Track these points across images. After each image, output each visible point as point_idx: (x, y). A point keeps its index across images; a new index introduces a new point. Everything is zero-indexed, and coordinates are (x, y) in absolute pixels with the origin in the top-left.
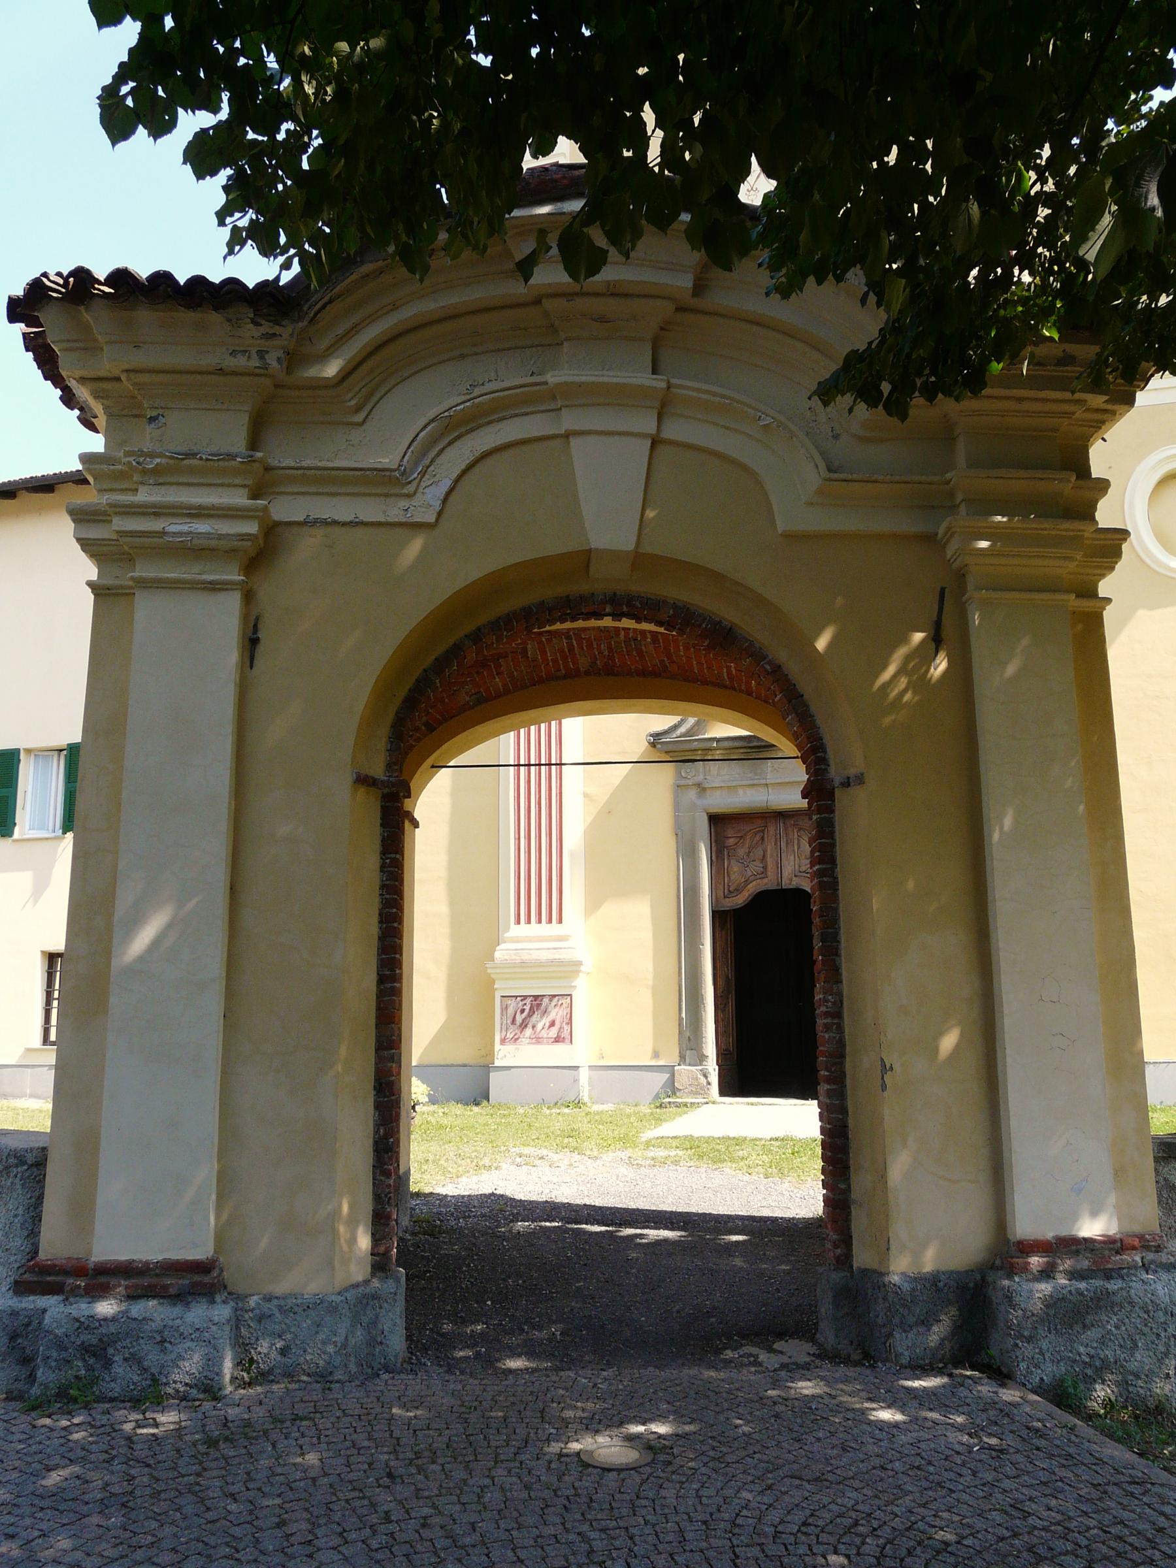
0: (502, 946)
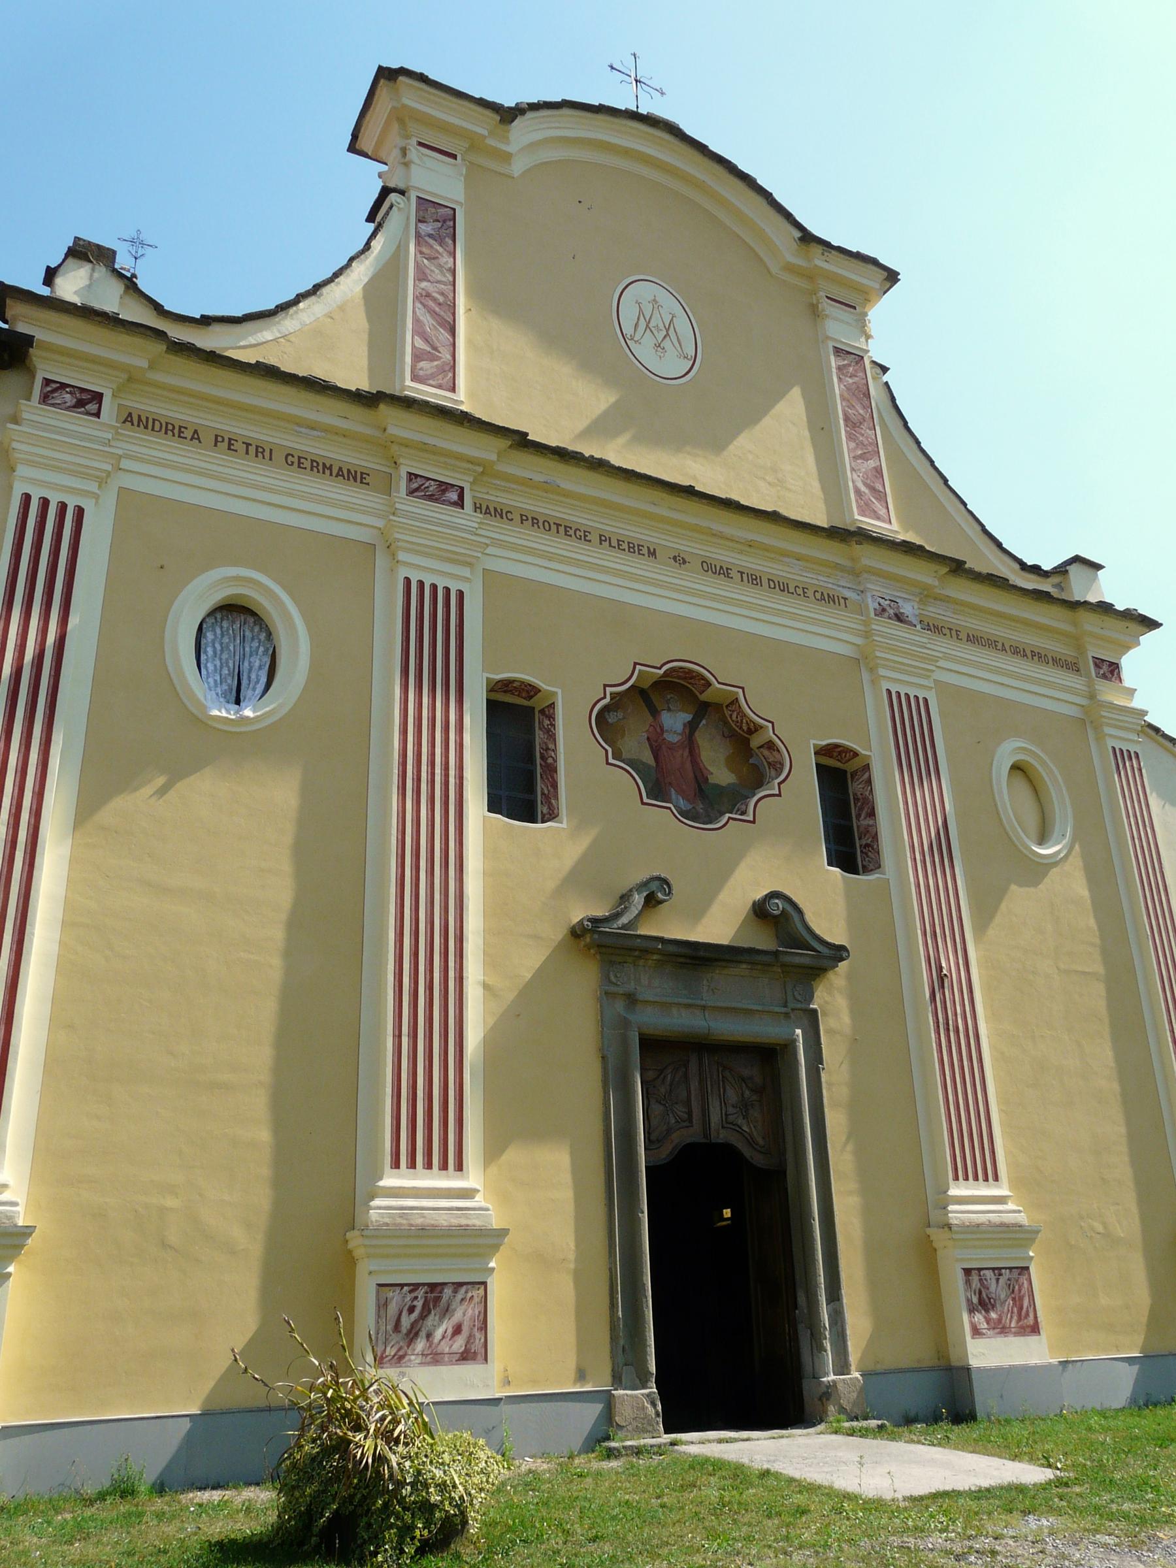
0: (377, 1202)
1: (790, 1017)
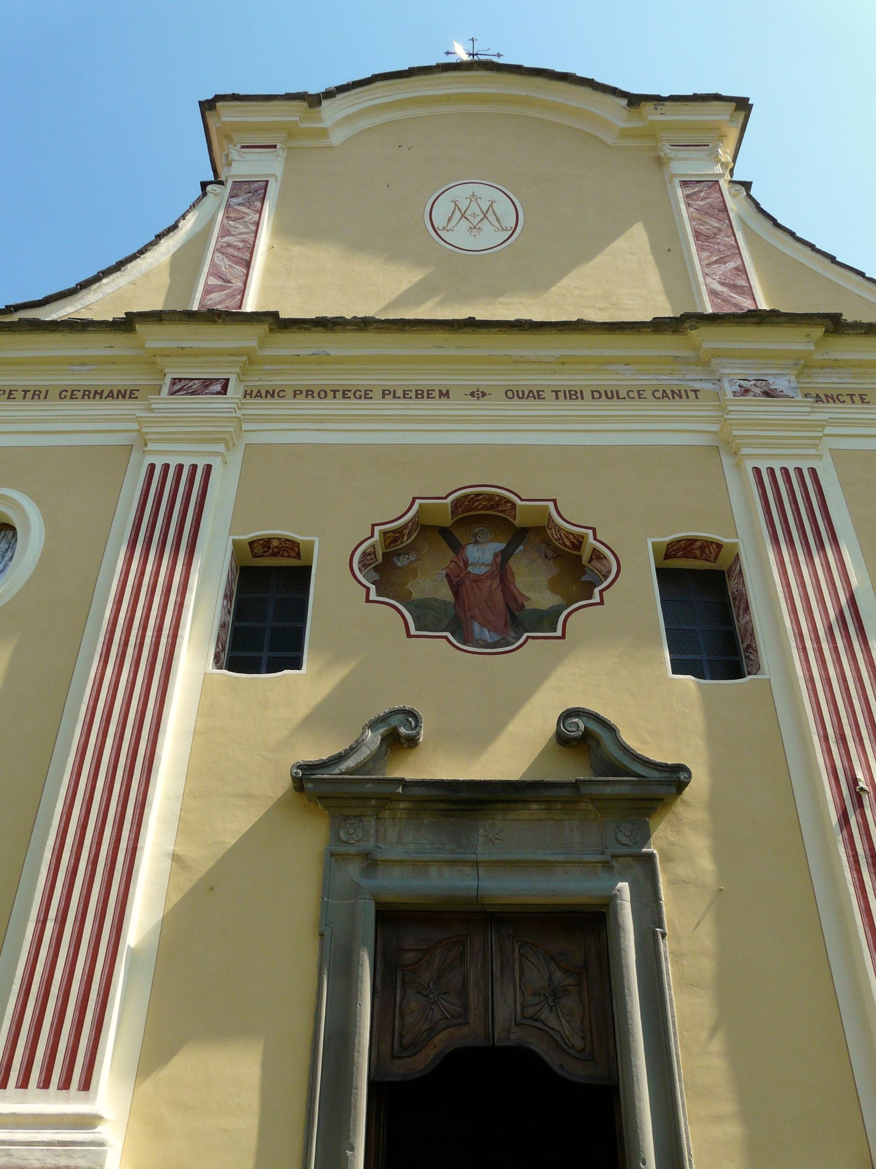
1: (613, 867)
